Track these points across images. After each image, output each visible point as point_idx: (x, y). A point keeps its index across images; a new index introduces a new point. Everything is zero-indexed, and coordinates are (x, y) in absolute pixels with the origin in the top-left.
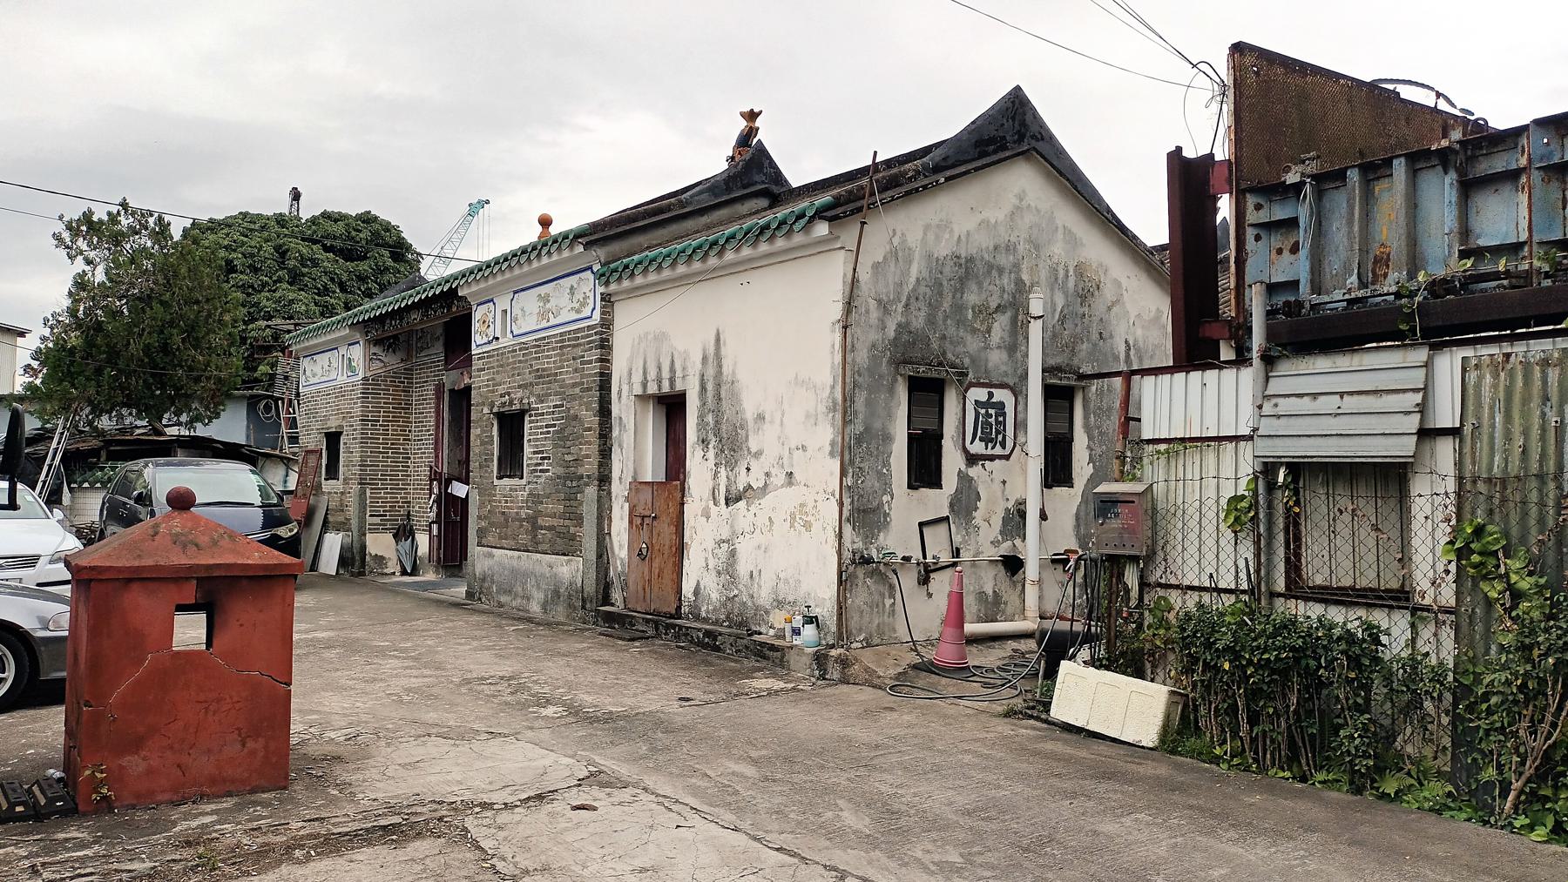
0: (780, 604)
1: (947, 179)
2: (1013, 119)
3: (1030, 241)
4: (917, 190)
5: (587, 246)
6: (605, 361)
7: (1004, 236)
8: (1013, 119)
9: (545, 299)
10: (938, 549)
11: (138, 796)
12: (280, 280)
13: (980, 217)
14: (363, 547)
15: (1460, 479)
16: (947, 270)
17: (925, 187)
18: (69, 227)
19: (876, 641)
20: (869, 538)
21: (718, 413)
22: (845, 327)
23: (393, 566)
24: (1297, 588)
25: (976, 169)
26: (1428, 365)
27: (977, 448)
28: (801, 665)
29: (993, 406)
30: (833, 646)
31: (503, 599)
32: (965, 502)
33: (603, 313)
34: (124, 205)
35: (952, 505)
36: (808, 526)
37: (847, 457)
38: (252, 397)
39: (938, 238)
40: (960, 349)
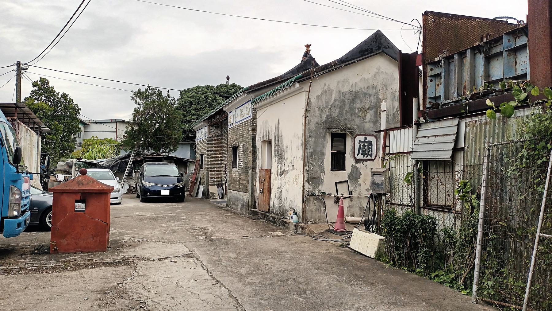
0: (290, 208)
1: (345, 65)
2: (376, 42)
3: (383, 84)
4: (333, 70)
5: (248, 93)
6: (254, 130)
7: (371, 83)
8: (376, 42)
9: (242, 111)
10: (343, 190)
11: (65, 250)
12: (206, 107)
13: (361, 77)
14: (208, 190)
15: (464, 166)
16: (347, 96)
17: (336, 69)
18: (135, 94)
19: (318, 221)
20: (315, 187)
21: (278, 146)
22: (305, 117)
23: (217, 196)
24: (428, 205)
25: (357, 61)
26: (458, 125)
27: (360, 157)
28: (292, 227)
29: (367, 142)
30: (301, 223)
31: (233, 206)
32: (355, 176)
33: (253, 115)
34: (149, 87)
35: (349, 177)
36: (297, 183)
37: (306, 160)
38: (192, 144)
39: (343, 86)
40: (353, 123)
